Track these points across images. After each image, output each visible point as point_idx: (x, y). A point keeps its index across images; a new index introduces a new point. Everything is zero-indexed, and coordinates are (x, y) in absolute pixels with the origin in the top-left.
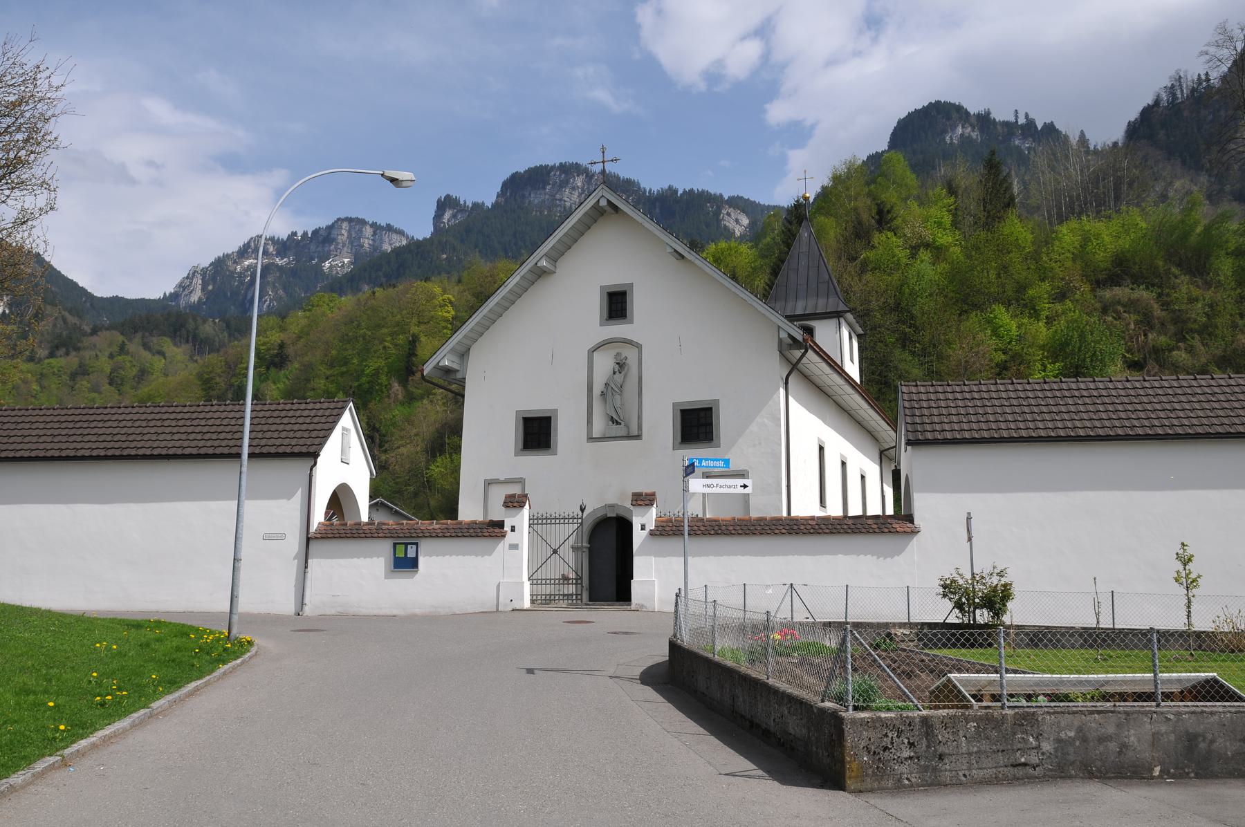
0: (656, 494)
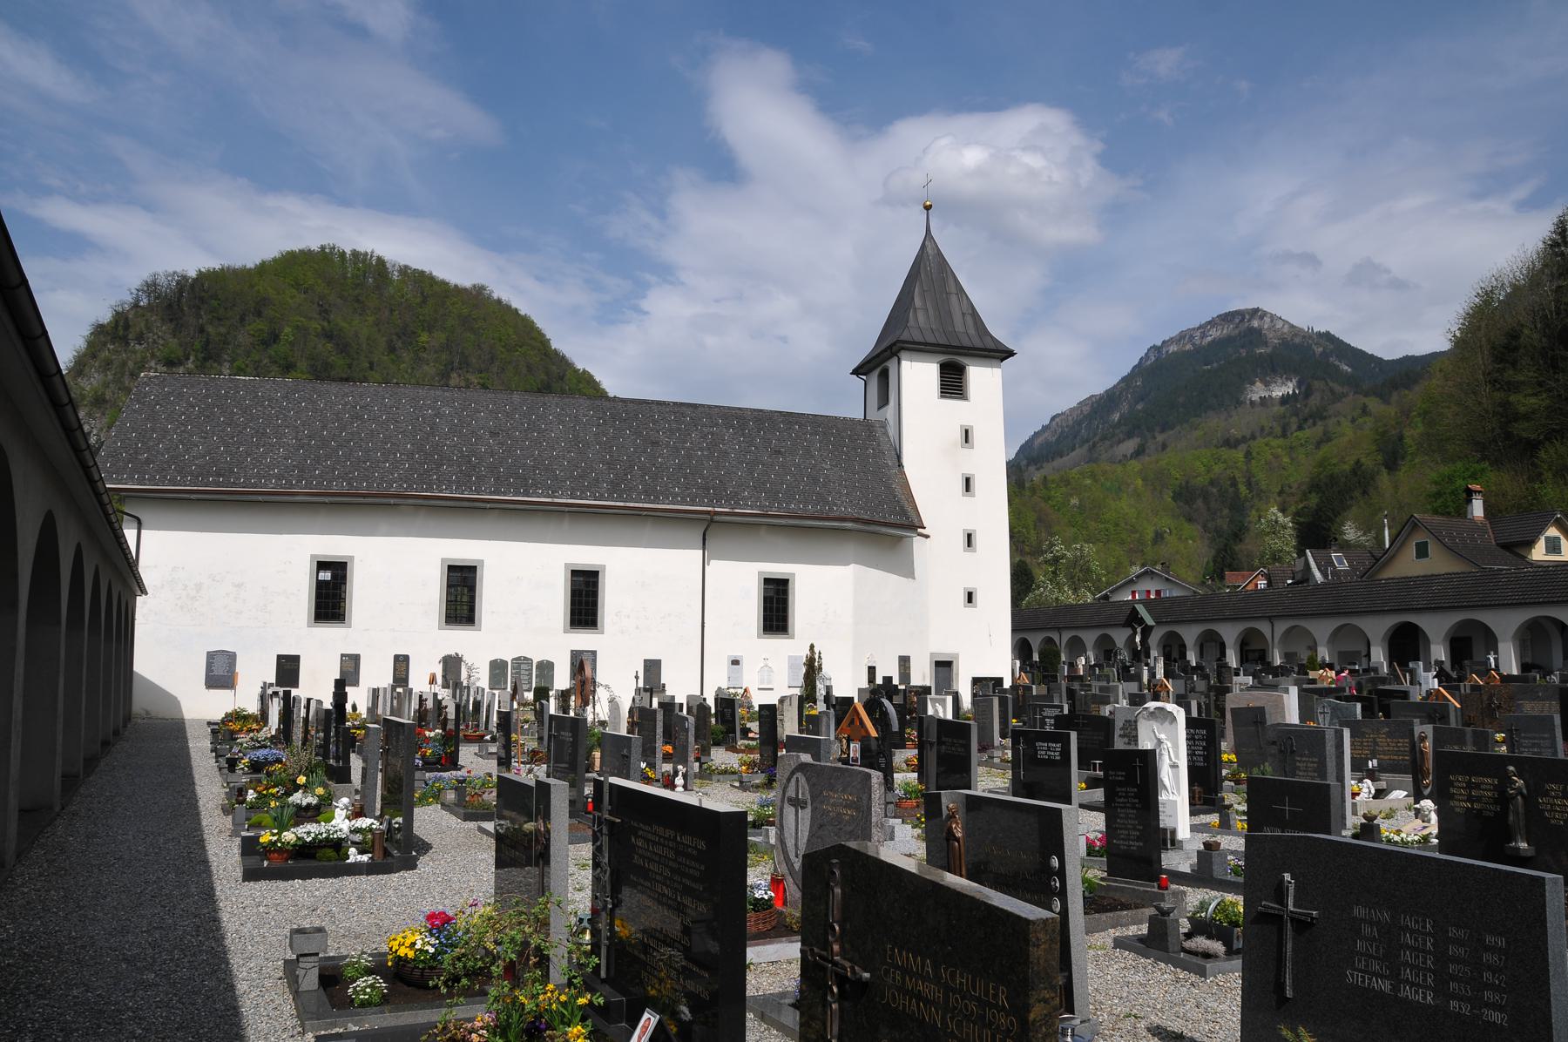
0: (239, 873)
